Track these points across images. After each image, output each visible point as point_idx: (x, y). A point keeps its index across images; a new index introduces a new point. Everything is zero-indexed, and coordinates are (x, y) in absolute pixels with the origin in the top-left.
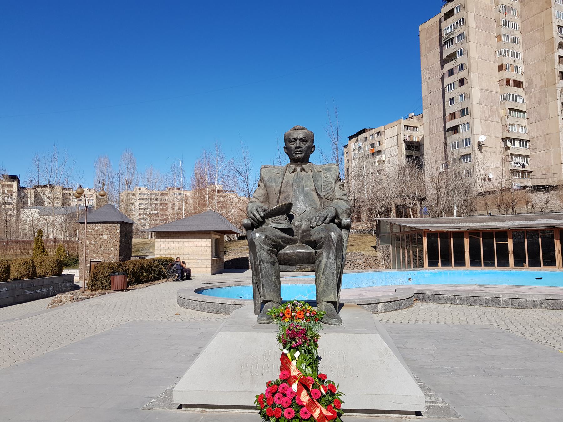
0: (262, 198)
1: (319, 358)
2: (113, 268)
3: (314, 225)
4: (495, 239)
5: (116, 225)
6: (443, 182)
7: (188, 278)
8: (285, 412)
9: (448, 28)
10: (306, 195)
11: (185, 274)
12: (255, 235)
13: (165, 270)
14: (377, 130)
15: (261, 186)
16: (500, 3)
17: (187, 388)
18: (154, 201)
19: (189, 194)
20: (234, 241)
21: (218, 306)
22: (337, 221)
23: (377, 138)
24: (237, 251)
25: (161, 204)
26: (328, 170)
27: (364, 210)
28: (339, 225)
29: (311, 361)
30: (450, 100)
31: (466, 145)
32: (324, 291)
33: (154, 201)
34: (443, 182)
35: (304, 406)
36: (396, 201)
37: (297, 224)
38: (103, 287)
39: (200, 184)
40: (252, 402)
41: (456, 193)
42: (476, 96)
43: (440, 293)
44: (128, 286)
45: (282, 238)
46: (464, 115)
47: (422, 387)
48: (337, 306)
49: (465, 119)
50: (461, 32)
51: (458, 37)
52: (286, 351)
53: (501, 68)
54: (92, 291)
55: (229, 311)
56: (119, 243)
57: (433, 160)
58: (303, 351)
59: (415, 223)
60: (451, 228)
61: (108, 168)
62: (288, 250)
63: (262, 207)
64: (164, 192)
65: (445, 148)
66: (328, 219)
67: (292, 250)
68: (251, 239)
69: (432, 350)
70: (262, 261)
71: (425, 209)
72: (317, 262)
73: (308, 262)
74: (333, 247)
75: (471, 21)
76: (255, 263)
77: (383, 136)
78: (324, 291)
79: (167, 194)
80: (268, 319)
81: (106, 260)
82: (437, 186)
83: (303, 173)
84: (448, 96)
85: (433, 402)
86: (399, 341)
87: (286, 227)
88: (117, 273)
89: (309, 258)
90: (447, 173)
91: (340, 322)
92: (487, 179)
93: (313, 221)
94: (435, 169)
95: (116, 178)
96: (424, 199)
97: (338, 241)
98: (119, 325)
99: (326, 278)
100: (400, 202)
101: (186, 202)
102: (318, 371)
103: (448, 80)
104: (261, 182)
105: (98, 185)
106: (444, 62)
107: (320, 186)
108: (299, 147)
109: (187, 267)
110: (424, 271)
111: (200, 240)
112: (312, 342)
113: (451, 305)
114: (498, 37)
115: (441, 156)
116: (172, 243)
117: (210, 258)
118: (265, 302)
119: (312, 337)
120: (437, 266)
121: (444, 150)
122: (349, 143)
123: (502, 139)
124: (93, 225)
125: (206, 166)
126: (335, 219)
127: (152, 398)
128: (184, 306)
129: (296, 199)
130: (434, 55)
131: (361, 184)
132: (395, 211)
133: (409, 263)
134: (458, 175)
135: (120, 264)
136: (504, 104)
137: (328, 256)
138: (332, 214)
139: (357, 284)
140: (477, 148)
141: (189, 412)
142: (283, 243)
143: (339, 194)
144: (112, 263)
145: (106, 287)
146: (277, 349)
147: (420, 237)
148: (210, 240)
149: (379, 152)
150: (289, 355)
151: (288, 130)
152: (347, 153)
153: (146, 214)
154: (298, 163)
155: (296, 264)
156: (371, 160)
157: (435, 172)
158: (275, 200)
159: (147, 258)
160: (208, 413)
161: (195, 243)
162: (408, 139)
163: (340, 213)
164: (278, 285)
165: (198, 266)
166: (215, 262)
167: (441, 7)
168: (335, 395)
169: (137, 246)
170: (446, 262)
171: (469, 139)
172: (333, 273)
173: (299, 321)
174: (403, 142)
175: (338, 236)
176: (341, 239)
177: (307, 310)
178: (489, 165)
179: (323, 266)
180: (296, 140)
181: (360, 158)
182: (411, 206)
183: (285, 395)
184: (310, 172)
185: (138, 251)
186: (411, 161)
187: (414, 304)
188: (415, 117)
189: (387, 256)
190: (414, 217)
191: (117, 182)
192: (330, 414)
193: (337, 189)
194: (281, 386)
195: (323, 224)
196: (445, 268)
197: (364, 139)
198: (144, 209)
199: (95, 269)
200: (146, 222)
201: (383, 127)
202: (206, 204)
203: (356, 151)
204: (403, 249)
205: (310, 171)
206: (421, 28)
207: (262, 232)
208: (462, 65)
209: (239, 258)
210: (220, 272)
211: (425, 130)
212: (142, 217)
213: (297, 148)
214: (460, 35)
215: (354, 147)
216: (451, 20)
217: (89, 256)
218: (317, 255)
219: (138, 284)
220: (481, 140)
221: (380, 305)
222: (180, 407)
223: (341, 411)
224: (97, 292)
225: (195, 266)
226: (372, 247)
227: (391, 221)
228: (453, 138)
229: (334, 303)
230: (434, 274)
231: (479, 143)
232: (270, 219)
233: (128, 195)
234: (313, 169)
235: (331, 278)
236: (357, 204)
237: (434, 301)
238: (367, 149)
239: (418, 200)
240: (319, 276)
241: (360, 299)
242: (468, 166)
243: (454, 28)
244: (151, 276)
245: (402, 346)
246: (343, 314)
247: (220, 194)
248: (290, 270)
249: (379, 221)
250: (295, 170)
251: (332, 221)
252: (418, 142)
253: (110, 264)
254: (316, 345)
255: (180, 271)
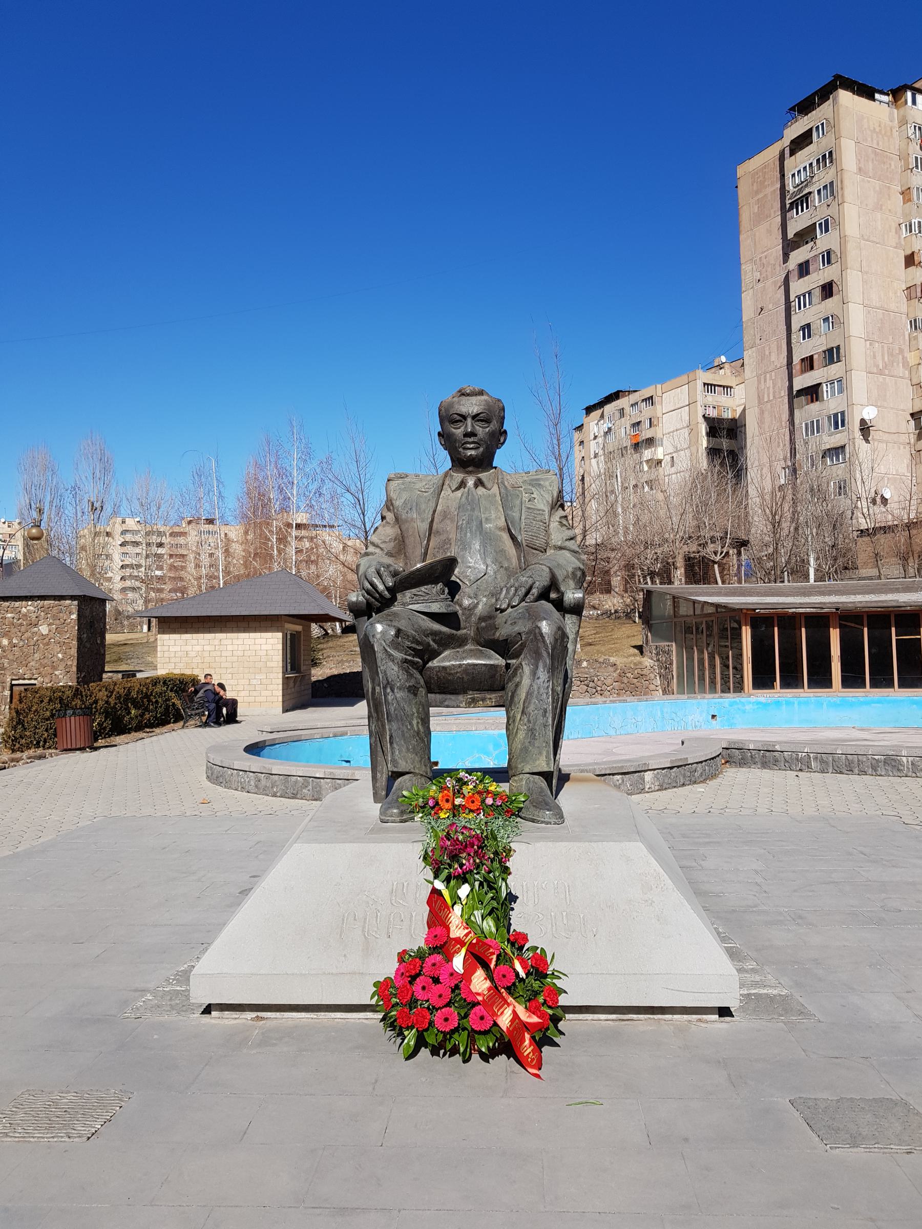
0: (390, 546)
1: (512, 898)
2: (61, 699)
3: (504, 606)
4: (893, 629)
5: (68, 602)
6: (786, 507)
7: (232, 718)
8: (437, 1017)
9: (799, 172)
10: (487, 539)
11: (224, 711)
12: (374, 629)
13: (178, 703)
14: (646, 393)
15: (388, 519)
16: (910, 120)
17: (219, 972)
18: (154, 549)
19: (235, 532)
20: (335, 636)
21: (296, 782)
22: (553, 595)
23: (647, 411)
24: (337, 660)
25: (171, 556)
26: (536, 483)
27: (616, 568)
28: (559, 605)
29: (495, 904)
30: (803, 328)
31: (836, 427)
32: (525, 750)
33: (154, 549)
34: (786, 507)
35: (478, 1003)
36: (686, 548)
37: (466, 602)
38: (38, 743)
39: (258, 512)
40: (366, 996)
41: (814, 530)
42: (857, 321)
43: (778, 748)
44: (96, 740)
45: (434, 633)
46: (831, 361)
47: (733, 954)
48: (554, 782)
49: (835, 370)
50: (826, 180)
51: (819, 191)
52: (439, 885)
53: (910, 260)
54: (13, 751)
55: (319, 792)
56: (75, 643)
57: (765, 460)
58: (477, 883)
59: (726, 595)
60: (801, 605)
61: (50, 474)
62: (446, 660)
63: (389, 566)
64: (177, 529)
65: (792, 433)
66: (535, 591)
67: (456, 660)
68: (366, 636)
69: (756, 872)
70: (389, 684)
71: (748, 565)
72: (511, 686)
73: (490, 686)
74: (545, 654)
75: (848, 157)
76: (374, 689)
77: (658, 407)
78: (525, 750)
79: (183, 534)
80: (402, 813)
81: (47, 680)
82: (774, 516)
83: (481, 490)
84: (798, 321)
85: (755, 984)
86: (689, 860)
87: (443, 610)
88: (70, 712)
89: (493, 676)
90: (795, 487)
91: (560, 816)
92: (878, 500)
93: (502, 596)
94: (769, 478)
95: (68, 497)
96: (744, 543)
97: (556, 640)
98: (74, 828)
99: (529, 721)
100: (694, 549)
101: (227, 551)
102: (510, 924)
103: (798, 287)
104: (389, 510)
105: (26, 513)
106: (789, 246)
107: (517, 518)
108: (473, 434)
109: (229, 695)
110: (743, 700)
111: (258, 635)
112: (496, 865)
113: (800, 774)
114: (906, 193)
115: (782, 450)
116: (195, 642)
117: (280, 675)
118: (396, 775)
119: (496, 853)
120: (772, 687)
121: (788, 438)
122: (586, 420)
123: (912, 415)
124: (17, 604)
125: (271, 470)
126: (550, 592)
127: (144, 991)
128: (220, 784)
129: (464, 549)
130: (769, 231)
131: (611, 512)
132: (683, 570)
133: (713, 681)
134: (817, 492)
135: (77, 689)
136: (916, 338)
137: (534, 673)
138: (542, 581)
139: (603, 729)
140: (858, 434)
141: (226, 1022)
142: (436, 646)
143: (557, 536)
144: (58, 689)
145: (45, 742)
146: (420, 880)
147: (736, 625)
148: (280, 635)
149: (650, 442)
150: (446, 894)
151: (447, 395)
152: (582, 443)
153: (136, 578)
154: (470, 469)
155: (464, 691)
156: (631, 458)
157: (768, 487)
158: (419, 551)
159: (139, 675)
160: (268, 1023)
161: (247, 642)
162: (713, 413)
163: (560, 578)
164: (424, 737)
165: (254, 693)
166: (292, 684)
167: (785, 126)
168: (545, 976)
169: (116, 649)
170: (791, 680)
171: (843, 413)
172: (545, 711)
173: (471, 816)
174: (701, 420)
175: (555, 629)
176: (561, 637)
177: (488, 792)
178: (883, 470)
179: (523, 696)
180: (464, 417)
181: (609, 456)
182: (718, 558)
183: (436, 981)
184: (495, 490)
185: (119, 660)
186: (717, 462)
187: (721, 772)
188: (727, 366)
189: (666, 667)
190: (723, 582)
191: (70, 508)
192: (535, 1019)
193: (554, 525)
194: (430, 960)
195: (523, 604)
196: (790, 693)
197: (617, 415)
198: (131, 566)
199: (21, 701)
200: (137, 595)
201: (659, 386)
202: (271, 556)
203: (600, 440)
204: (701, 652)
205: (496, 488)
206: (741, 170)
207: (389, 621)
208: (829, 253)
209: (335, 676)
210: (303, 706)
211: (751, 392)
212: (128, 583)
213: (467, 435)
214: (825, 187)
215: (596, 429)
216: (806, 156)
217: (8, 673)
218: (511, 671)
219: (119, 734)
220: (866, 417)
221: (648, 776)
222: (208, 1010)
223: (559, 1012)
224: (25, 755)
225: (247, 693)
226: (635, 647)
227: (674, 592)
228: (808, 412)
229: (547, 776)
230: (765, 705)
231: (863, 421)
232: (408, 594)
233: (97, 534)
234: (503, 483)
235: (541, 720)
236: (603, 554)
237: (765, 765)
238: (623, 433)
239: (732, 545)
240: (514, 717)
241: (605, 763)
242: (839, 472)
243: (812, 172)
244: (147, 716)
245: (694, 864)
246: (567, 799)
247: (303, 533)
248: (454, 704)
249: (649, 594)
250: (462, 484)
251: (544, 595)
252: (734, 420)
253: (53, 690)
254: (506, 871)
255: (213, 705)
